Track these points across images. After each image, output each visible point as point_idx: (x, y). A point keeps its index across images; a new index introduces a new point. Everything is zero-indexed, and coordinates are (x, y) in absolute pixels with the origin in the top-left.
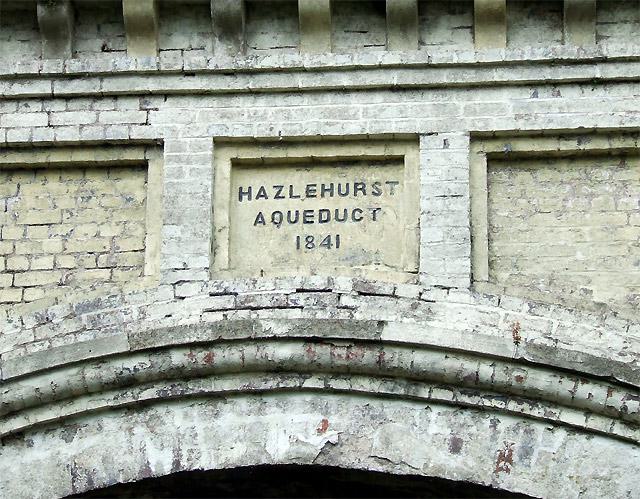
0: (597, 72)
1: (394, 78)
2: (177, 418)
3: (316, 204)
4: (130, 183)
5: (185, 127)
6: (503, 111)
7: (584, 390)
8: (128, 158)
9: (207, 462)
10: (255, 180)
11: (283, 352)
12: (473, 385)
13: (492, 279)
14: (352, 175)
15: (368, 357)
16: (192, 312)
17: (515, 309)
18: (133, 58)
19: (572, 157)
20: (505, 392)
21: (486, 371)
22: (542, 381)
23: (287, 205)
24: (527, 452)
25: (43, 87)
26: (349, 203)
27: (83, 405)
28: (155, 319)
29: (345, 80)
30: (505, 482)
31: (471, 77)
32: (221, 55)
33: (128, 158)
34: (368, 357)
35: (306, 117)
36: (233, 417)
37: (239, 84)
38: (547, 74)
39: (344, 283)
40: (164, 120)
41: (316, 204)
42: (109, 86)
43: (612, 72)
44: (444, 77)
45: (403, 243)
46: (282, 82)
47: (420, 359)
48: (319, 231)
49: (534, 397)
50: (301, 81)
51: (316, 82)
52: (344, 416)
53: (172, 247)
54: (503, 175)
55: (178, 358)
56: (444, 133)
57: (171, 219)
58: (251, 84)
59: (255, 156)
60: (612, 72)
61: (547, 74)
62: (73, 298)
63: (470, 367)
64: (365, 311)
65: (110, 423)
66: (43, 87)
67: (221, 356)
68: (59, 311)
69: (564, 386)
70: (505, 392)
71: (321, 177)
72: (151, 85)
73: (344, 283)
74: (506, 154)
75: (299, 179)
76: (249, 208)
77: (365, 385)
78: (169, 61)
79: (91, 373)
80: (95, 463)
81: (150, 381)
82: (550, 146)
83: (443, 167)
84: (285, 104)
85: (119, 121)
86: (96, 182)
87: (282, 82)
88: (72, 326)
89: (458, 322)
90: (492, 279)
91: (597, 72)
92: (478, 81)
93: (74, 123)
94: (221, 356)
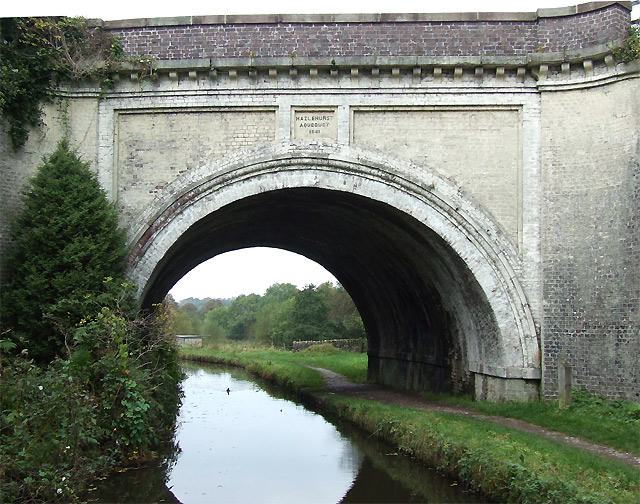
0: (379, 91)
1: (332, 91)
2: (283, 175)
3: (314, 122)
4: (271, 115)
5: (284, 102)
6: (357, 100)
7: (373, 171)
8: (271, 110)
9: (290, 186)
10: (300, 115)
11: (307, 161)
12: (349, 169)
13: (354, 142)
14: (323, 114)
15: (326, 162)
16: (284, 150)
17: (359, 151)
18: (272, 85)
19: (373, 111)
20: (356, 171)
21: (351, 166)
22: (364, 169)
23: (307, 122)
24: (360, 185)
25: (251, 92)
26: (322, 122)
27: (262, 172)
28: (278, 152)
29: (320, 92)
30: (355, 192)
31: (350, 91)
32: (292, 84)
33: (271, 110)
34: (326, 162)
35: (312, 101)
36: (296, 175)
37: (296, 92)
38: (367, 91)
39: (320, 143)
40: (279, 100)
41: (314, 122)
42: (266, 92)
43: (383, 91)
44: (344, 92)
45: (411, 364)
46: (306, 92)
47: (337, 163)
48: (315, 129)
49: (362, 172)
50: (311, 91)
51: (314, 92)
52: (320, 175)
53: (282, 134)
54: (357, 115)
55: (283, 162)
56: (344, 103)
57: (281, 126)
58: (298, 91)
59: (300, 110)
60: (383, 91)
61: (367, 91)
62: (259, 145)
63: (348, 165)
64: (326, 150)
65: (268, 176)
66: (251, 92)
67: (293, 161)
68: (256, 149)
69: (369, 170)
70: (356, 171)
71: (316, 115)
72: (276, 92)
73: (320, 143)
74: (358, 111)
75: (310, 115)
76: (299, 122)
77: (325, 168)
78: (280, 85)
79: (264, 165)
80: (265, 185)
81: (277, 166)
82: (368, 109)
83: (343, 114)
84: (520, 85)
85: (268, 100)
86: (264, 115)
87: (306, 92)
88: (259, 153)
89: (346, 154)
90: (354, 142)
91: (379, 91)
92: (351, 92)
93: (258, 101)
94: (293, 161)
